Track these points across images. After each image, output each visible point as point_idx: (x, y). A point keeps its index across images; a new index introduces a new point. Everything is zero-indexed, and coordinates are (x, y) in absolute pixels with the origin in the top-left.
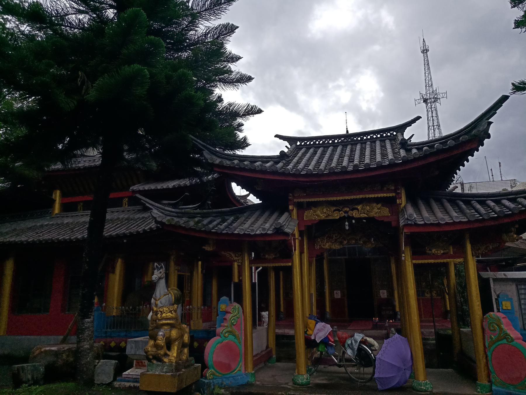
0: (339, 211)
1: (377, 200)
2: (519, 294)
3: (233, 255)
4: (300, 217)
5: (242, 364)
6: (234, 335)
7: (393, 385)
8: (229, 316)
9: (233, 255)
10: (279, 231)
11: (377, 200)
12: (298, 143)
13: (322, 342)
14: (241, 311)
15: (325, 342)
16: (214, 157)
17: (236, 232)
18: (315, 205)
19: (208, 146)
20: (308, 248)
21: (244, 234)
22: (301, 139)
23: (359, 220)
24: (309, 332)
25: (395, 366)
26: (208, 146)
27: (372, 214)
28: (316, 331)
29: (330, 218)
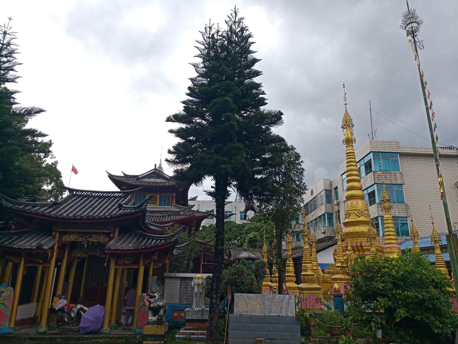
0: (82, 237)
1: (103, 233)
2: (181, 285)
3: (13, 258)
4: (60, 238)
5: (7, 322)
6: (5, 305)
7: (90, 330)
8: (4, 294)
9: (13, 258)
10: (39, 247)
11: (103, 233)
12: (75, 193)
13: (59, 310)
14: (13, 292)
15: (62, 309)
16: (8, 203)
17: (14, 247)
18: (70, 233)
19: (6, 197)
20: (68, 256)
21: (19, 248)
22: (77, 191)
23: (93, 243)
24: (54, 304)
25: (91, 320)
26: (6, 197)
27: (100, 240)
28: (57, 304)
29: (77, 240)
